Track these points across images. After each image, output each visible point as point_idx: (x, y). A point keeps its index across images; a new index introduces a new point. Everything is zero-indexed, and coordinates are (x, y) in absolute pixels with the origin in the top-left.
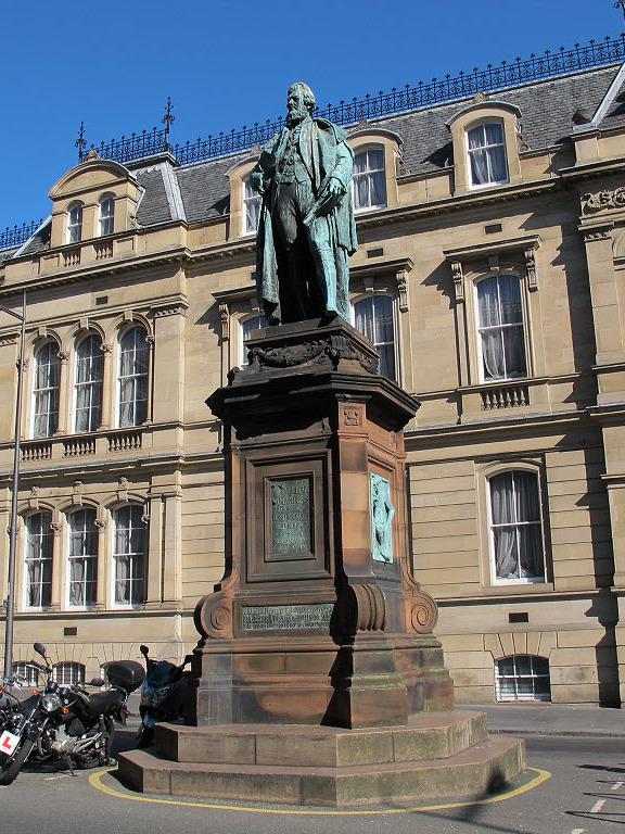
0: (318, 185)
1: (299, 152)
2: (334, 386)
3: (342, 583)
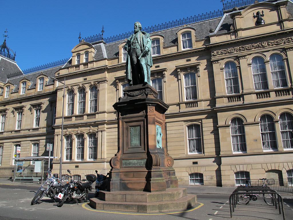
0: (142, 49)
1: (137, 40)
2: (146, 102)
3: (148, 154)
